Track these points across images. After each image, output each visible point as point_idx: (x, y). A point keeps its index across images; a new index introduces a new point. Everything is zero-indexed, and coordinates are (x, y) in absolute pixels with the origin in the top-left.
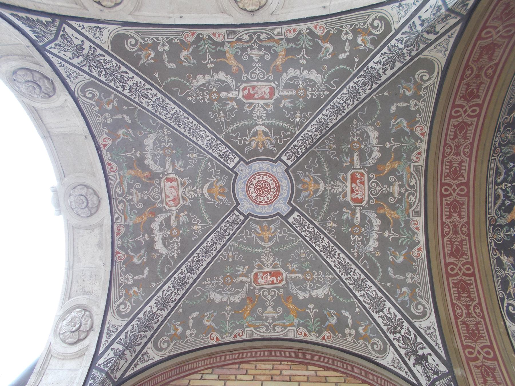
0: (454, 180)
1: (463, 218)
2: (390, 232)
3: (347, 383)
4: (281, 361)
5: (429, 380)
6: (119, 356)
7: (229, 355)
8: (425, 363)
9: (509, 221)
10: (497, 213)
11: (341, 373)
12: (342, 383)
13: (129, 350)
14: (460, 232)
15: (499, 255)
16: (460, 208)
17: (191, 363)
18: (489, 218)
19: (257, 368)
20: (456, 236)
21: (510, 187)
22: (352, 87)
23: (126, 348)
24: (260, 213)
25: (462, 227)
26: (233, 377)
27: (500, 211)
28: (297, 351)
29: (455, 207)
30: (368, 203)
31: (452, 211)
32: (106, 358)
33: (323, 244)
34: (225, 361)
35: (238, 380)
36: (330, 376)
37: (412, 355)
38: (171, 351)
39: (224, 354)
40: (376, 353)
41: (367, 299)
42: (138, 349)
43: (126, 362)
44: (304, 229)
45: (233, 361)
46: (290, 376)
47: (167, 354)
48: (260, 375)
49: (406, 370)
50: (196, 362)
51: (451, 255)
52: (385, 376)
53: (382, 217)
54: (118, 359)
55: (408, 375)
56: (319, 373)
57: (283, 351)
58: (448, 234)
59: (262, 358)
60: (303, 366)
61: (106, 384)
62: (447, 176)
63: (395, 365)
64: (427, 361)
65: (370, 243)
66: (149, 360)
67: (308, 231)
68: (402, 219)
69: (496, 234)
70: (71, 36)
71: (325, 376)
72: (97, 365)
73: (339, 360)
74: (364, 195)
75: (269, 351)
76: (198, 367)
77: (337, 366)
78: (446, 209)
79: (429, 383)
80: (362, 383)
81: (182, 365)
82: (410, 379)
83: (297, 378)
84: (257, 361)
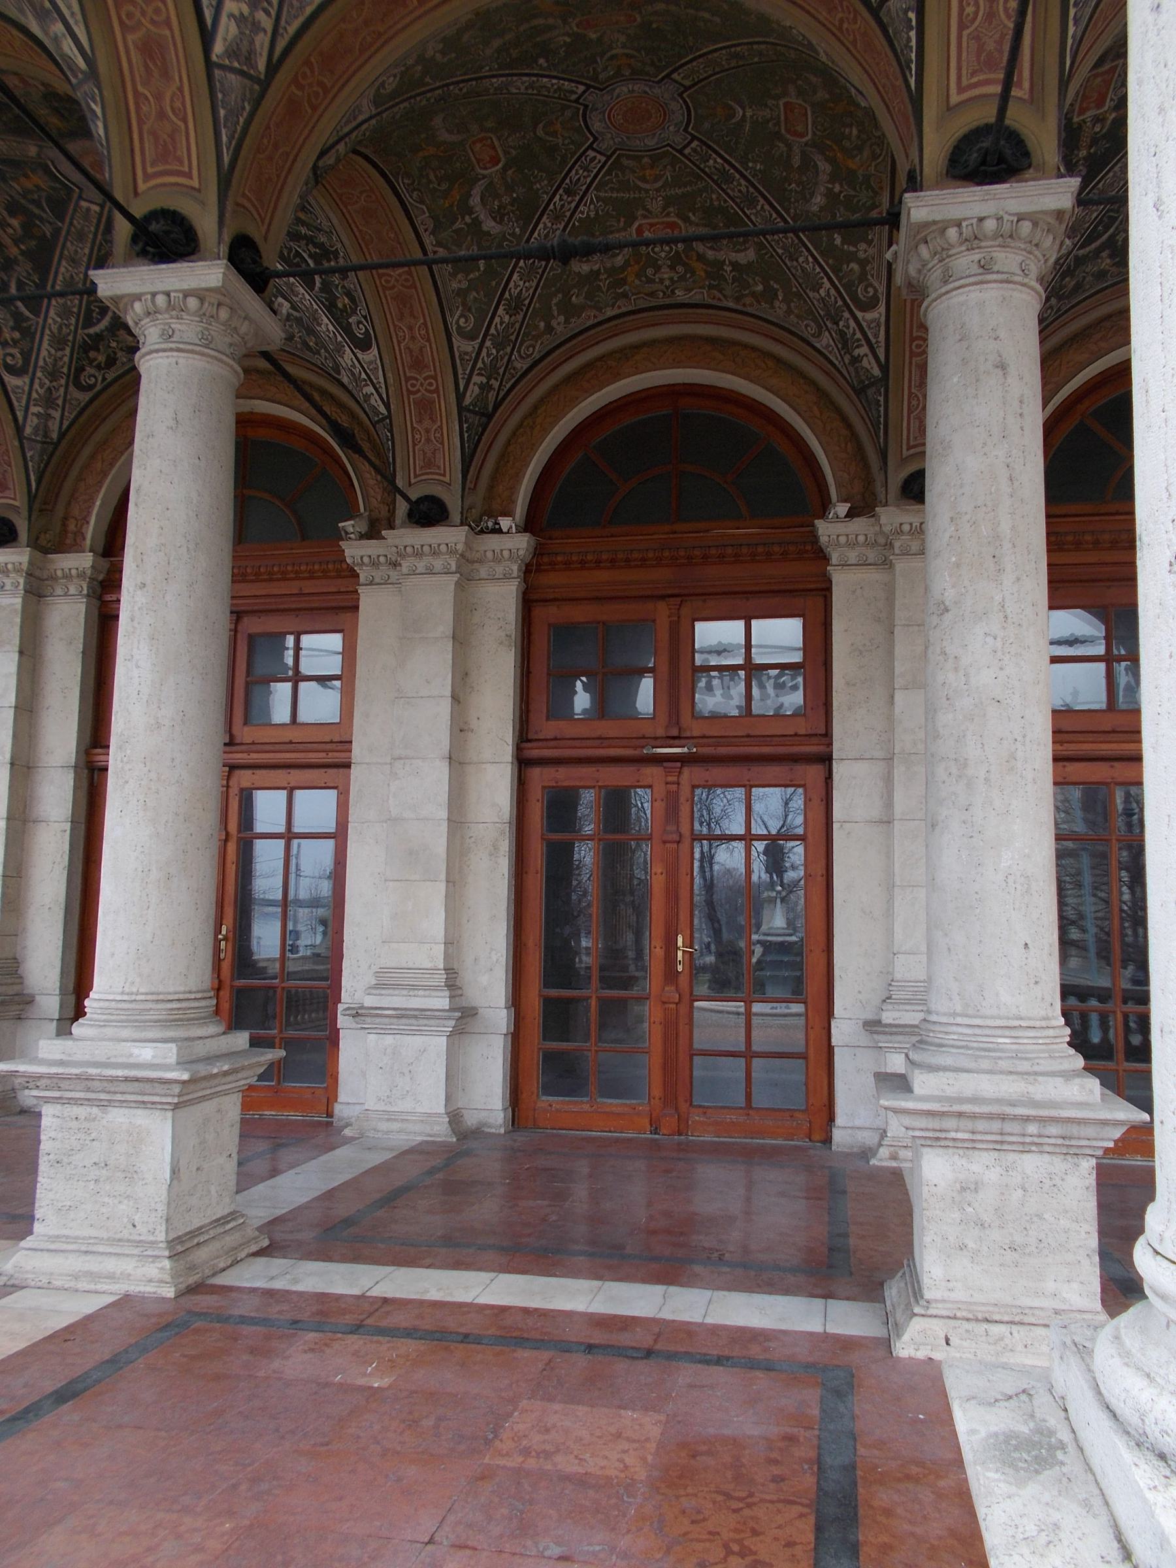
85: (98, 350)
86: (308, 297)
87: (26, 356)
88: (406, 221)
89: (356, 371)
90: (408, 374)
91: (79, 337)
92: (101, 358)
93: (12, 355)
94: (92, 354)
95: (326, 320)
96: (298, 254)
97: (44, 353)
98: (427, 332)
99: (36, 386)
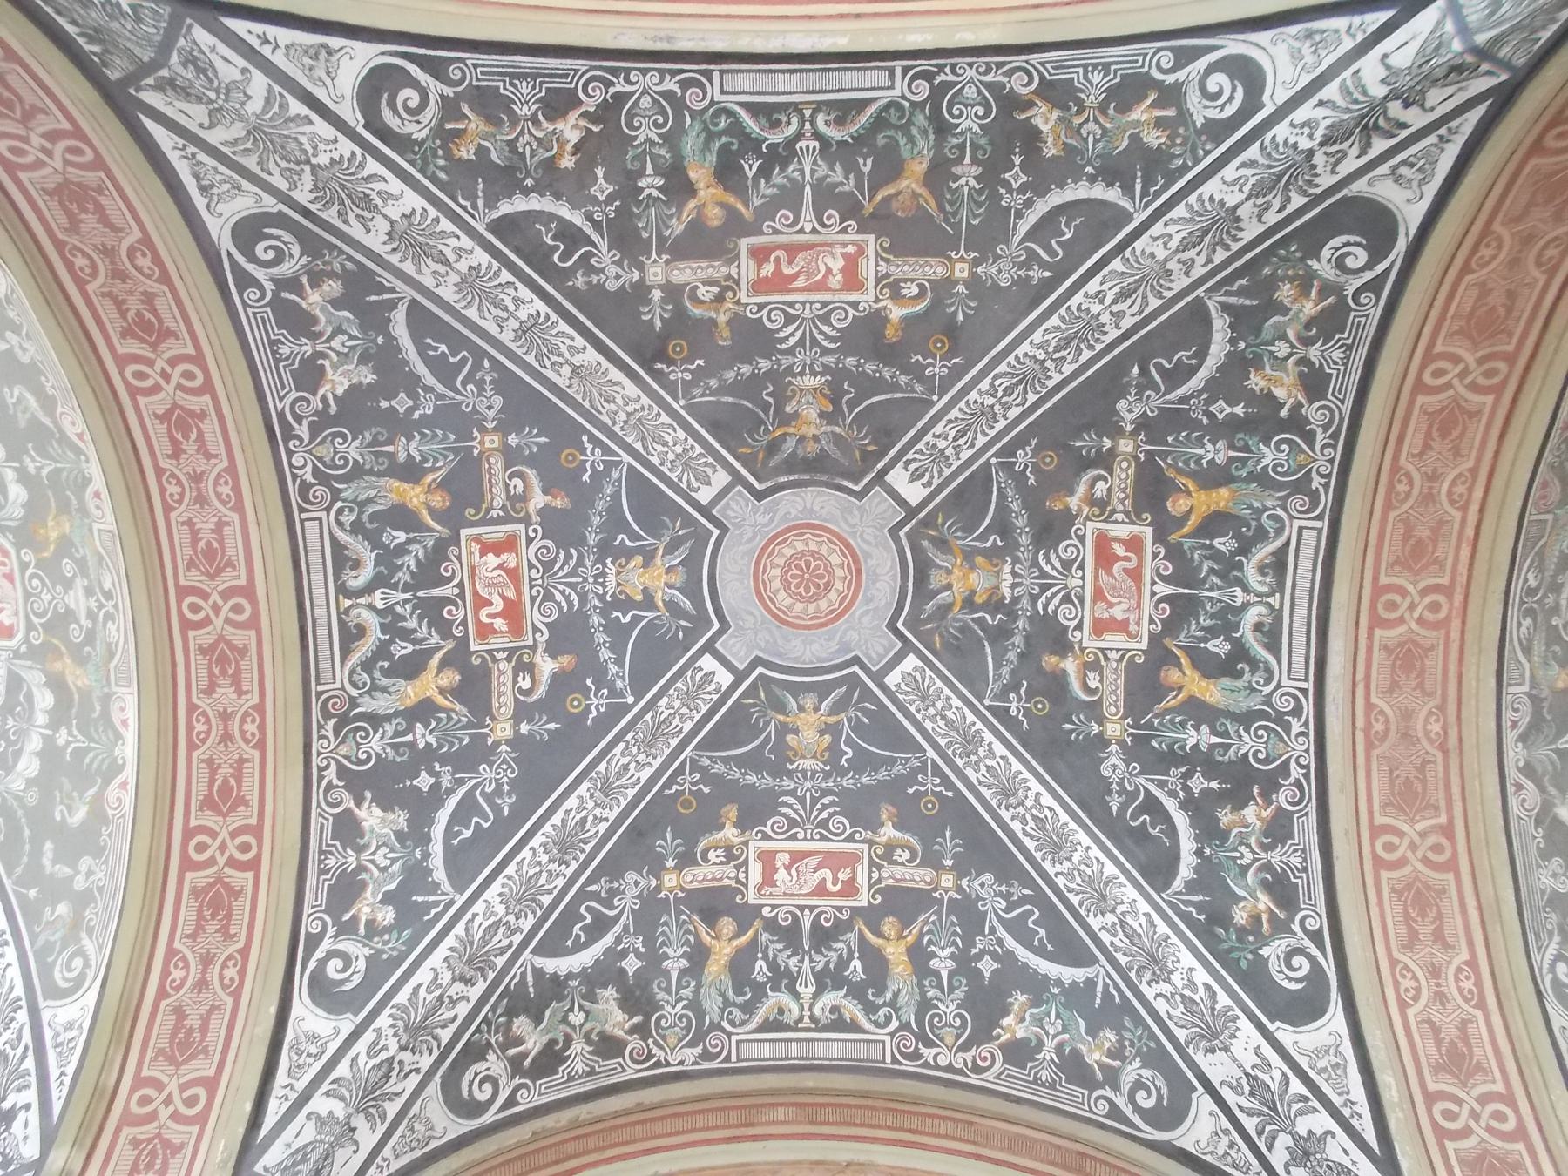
0: (212, 577)
1: (247, 692)
2: (70, 734)
9: (409, 703)
10: (355, 678)
14: (237, 734)
15: (352, 805)
16: (237, 662)
18: (319, 694)
20: (226, 746)
21: (406, 601)
22: (1143, 252)
24: (796, 660)
25: (243, 721)
27: (370, 674)
29: (223, 660)
30: (27, 640)
31: (216, 671)
32: (289, 1145)
33: (633, 765)
34: (603, 1148)
41: (1120, 940)
44: (932, 711)
51: (208, 803)
53: (57, 684)
58: (204, 741)
62: (190, 565)
65: (20, 766)
67: (944, 718)
68: (97, 693)
69: (350, 739)
70: (207, 51)
74: (16, 614)
78: (200, 665)
85: (537, 1019)
86: (1143, 906)
87: (378, 969)
88: (901, 1081)
89: (1273, 1079)
90: (1432, 1087)
91: (516, 969)
92: (534, 1042)
93: (347, 959)
94: (521, 1024)
95: (1188, 959)
96: (1152, 806)
97: (423, 976)
98: (1479, 983)
99: (361, 1046)
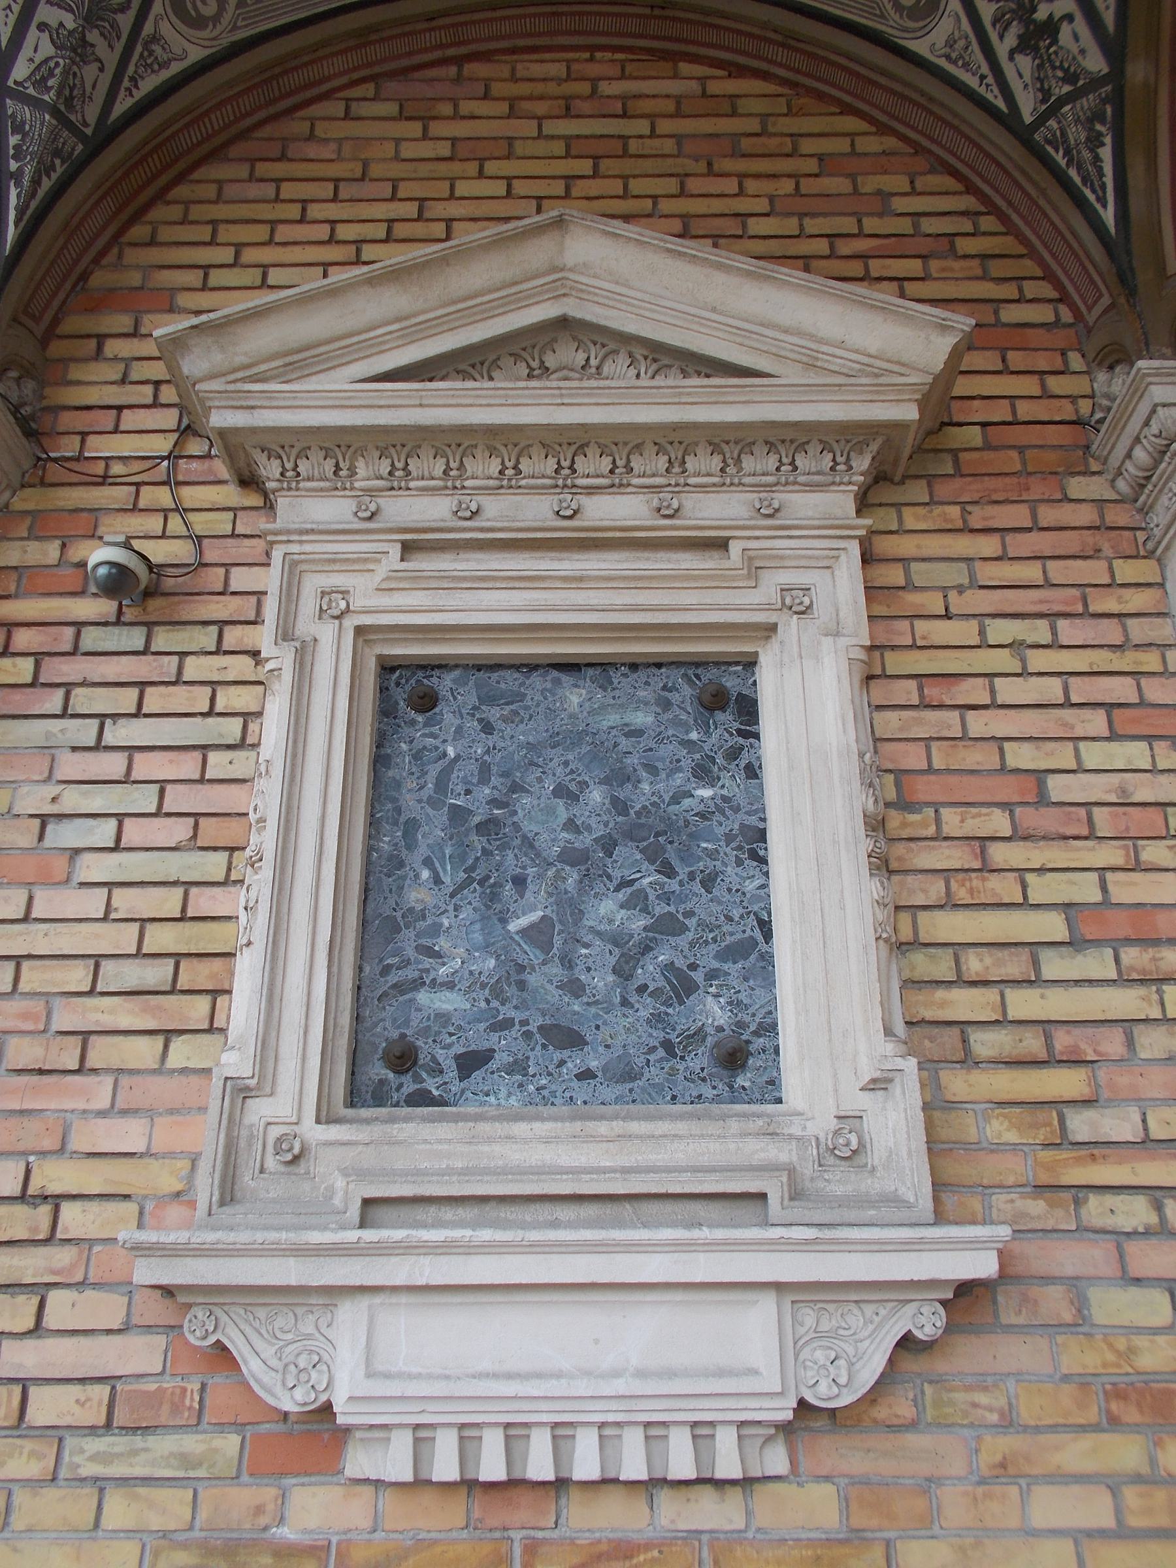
3: (796, 115)
4: (593, 48)
5: (1043, 101)
6: (74, 50)
7: (425, 31)
8: (1048, 48)
11: (780, 85)
12: (779, 115)
13: (97, 27)
17: (306, 65)
19: (518, 75)
23: (85, 19)
26: (446, 109)
28: (648, 11)
34: (410, 54)
35: (463, 118)
36: (746, 96)
37: (1015, 23)
38: (235, 28)
39: (407, 28)
40: (901, 17)
42: (125, 21)
43: (101, 70)
45: (438, 54)
46: (624, 98)
47: (222, 36)
48: (530, 98)
49: (985, 69)
50: (321, 59)
52: (916, 89)
54: (74, 63)
55: (987, 85)
56: (714, 87)
57: (600, 14)
59: (529, 42)
60: (662, 64)
61: (64, 144)
63: (954, 55)
64: (1055, 41)
66: (170, 60)
71: (731, 96)
72: (10, 83)
73: (780, 38)
75: (554, 14)
76: (328, 79)
77: (770, 62)
79: (1044, 107)
80: (841, 113)
81: (277, 70)
82: (990, 97)
83: (647, 106)
84: (513, 51)
